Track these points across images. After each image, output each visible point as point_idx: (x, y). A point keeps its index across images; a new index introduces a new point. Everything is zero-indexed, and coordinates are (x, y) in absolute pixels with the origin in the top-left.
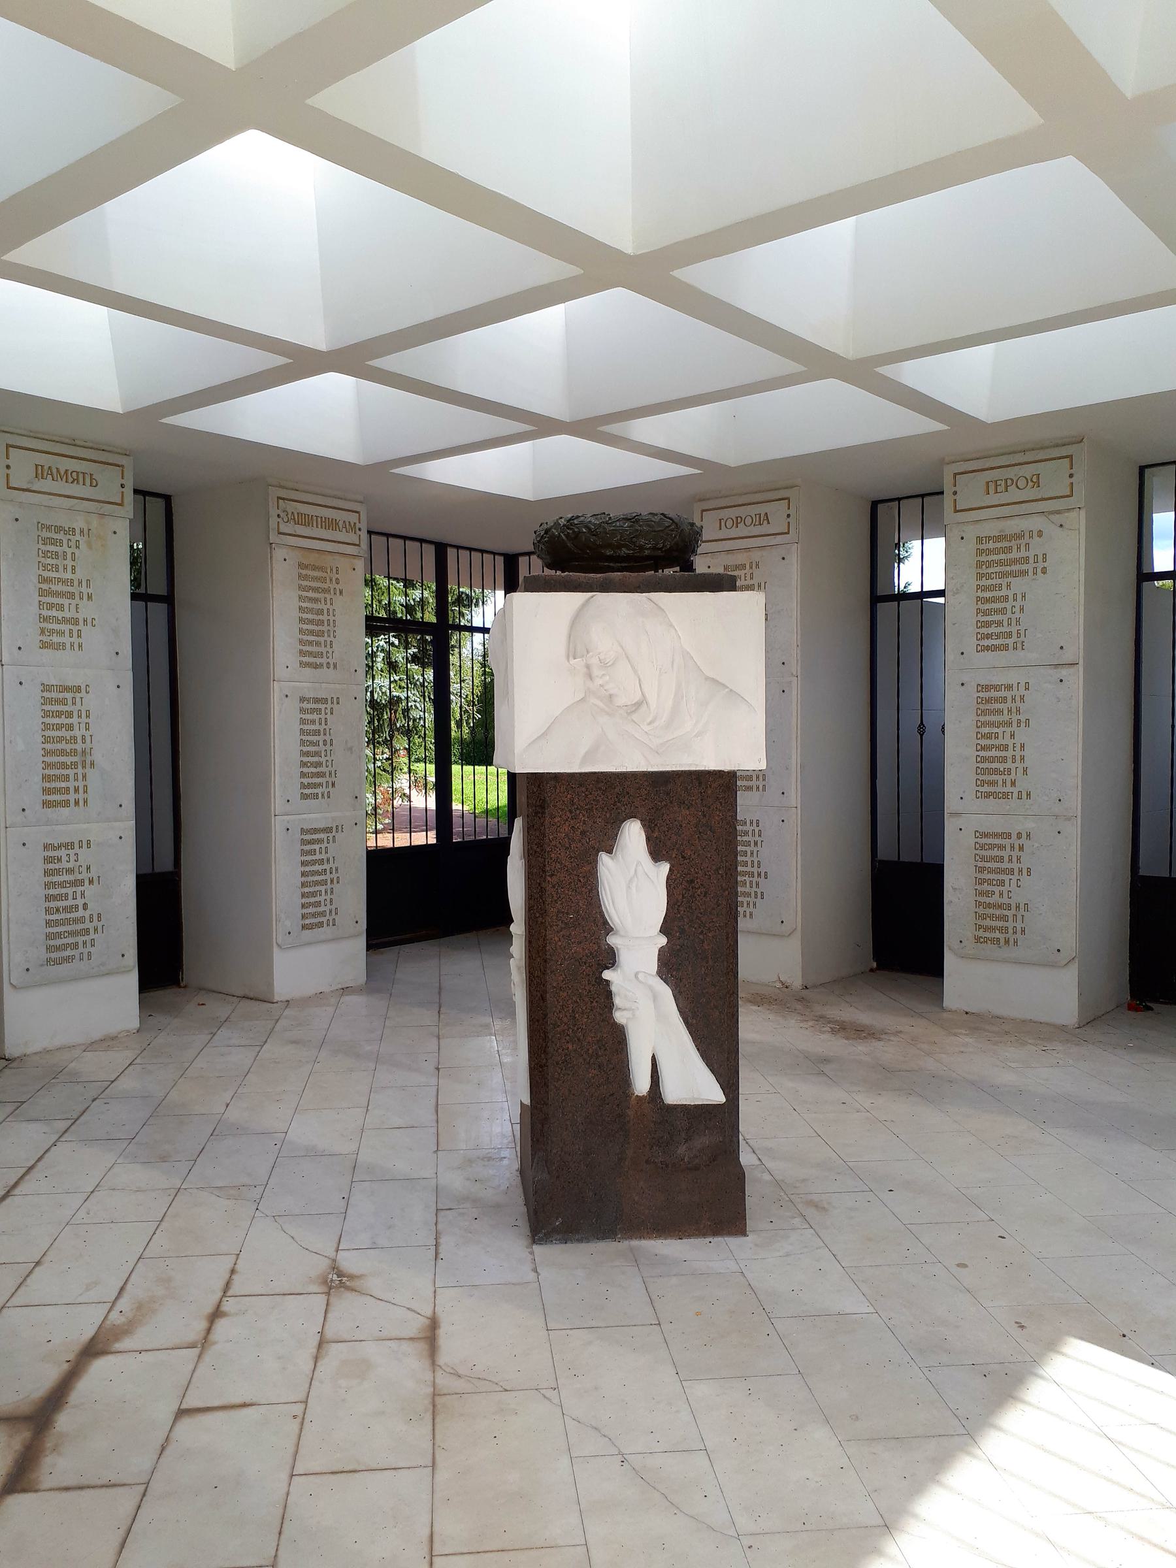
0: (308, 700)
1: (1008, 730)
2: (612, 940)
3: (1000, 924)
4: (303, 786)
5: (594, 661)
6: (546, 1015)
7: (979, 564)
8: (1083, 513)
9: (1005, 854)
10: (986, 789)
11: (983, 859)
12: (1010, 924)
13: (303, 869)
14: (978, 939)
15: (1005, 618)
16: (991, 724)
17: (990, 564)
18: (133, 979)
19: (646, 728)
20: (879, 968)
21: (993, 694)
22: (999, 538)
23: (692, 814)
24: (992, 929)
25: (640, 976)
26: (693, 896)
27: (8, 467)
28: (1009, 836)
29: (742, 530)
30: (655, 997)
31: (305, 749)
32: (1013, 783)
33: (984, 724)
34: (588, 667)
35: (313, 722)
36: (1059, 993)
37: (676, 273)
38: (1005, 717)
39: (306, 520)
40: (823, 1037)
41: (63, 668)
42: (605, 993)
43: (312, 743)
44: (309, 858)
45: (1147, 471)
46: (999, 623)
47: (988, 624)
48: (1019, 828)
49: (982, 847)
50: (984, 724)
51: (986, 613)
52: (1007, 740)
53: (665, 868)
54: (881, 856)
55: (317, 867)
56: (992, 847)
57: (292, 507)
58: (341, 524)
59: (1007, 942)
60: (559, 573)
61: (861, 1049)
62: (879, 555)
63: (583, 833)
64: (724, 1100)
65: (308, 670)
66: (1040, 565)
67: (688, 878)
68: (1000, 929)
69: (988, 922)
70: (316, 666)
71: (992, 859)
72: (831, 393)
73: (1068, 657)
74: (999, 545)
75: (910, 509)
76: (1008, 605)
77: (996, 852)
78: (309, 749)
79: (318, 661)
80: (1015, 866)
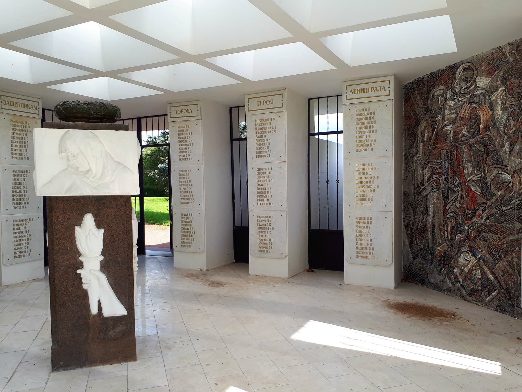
0: (16, 172)
1: (266, 183)
2: (81, 258)
3: (265, 246)
4: (14, 204)
5: (69, 154)
6: (55, 288)
7: (256, 129)
8: (286, 112)
9: (266, 223)
10: (260, 202)
11: (260, 225)
12: (268, 246)
13: (14, 235)
14: (259, 251)
15: (264, 147)
16: (261, 181)
17: (259, 129)
19: (92, 180)
20: (236, 262)
21: (261, 171)
22: (262, 120)
23: (110, 211)
24: (263, 247)
25: (92, 271)
26: (113, 241)
28: (267, 217)
29: (183, 114)
30: (98, 279)
31: (14, 190)
32: (268, 200)
33: (259, 181)
34: (68, 156)
35: (18, 180)
36: (281, 267)
37: (111, 17)
38: (265, 179)
39: (15, 104)
40: (205, 287)
42: (79, 278)
43: (18, 188)
44: (17, 231)
45: (311, 100)
46: (263, 148)
47: (259, 149)
48: (270, 215)
49: (260, 221)
50: (259, 181)
51: (259, 145)
52: (266, 186)
53: (102, 231)
54: (236, 225)
55: (21, 234)
56: (262, 221)
57: (7, 99)
58: (30, 106)
59: (267, 251)
60: (64, 122)
61: (215, 290)
63: (69, 219)
65: (16, 160)
66: (274, 129)
67: (112, 234)
68: (265, 247)
69: (262, 245)
70: (19, 159)
71: (263, 225)
72: (191, 68)
73: (283, 159)
74: (262, 123)
76: (265, 142)
77: (263, 223)
78: (16, 190)
79: (20, 157)
80: (269, 227)
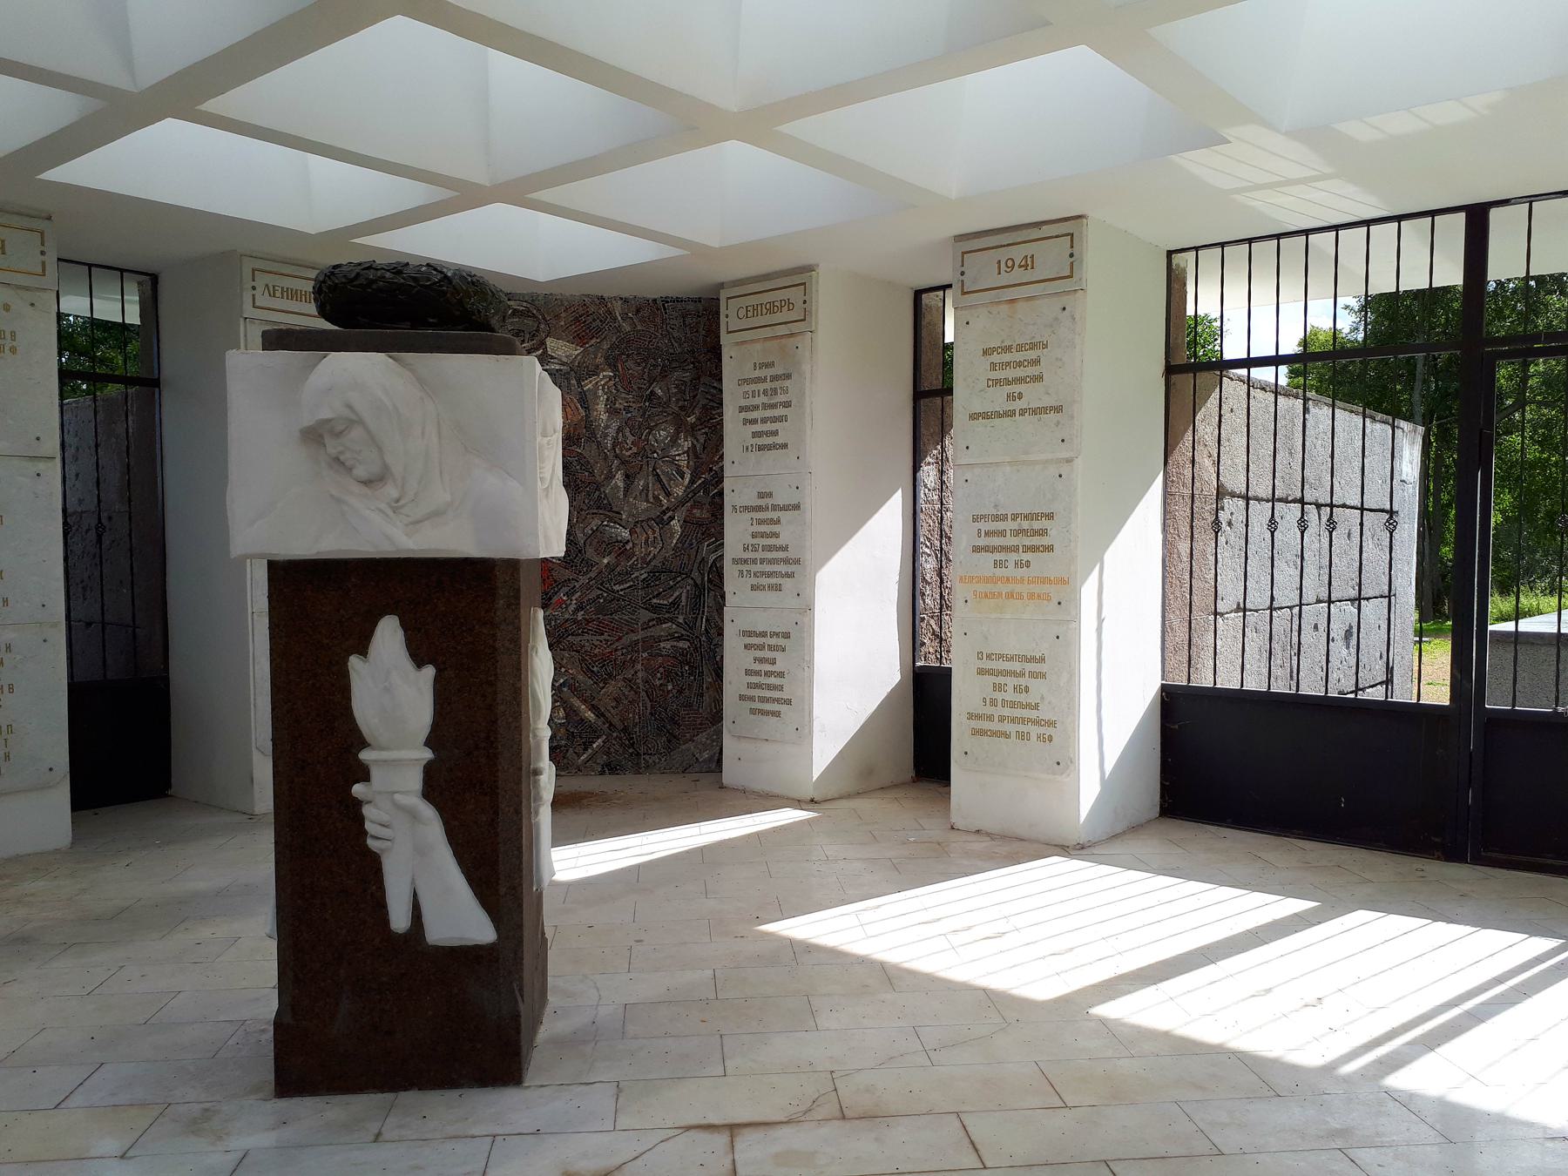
2: (365, 755)
18: (63, 795)
23: (454, 607)
27: (43, 253)
53: (429, 672)
75: (1210, 258)
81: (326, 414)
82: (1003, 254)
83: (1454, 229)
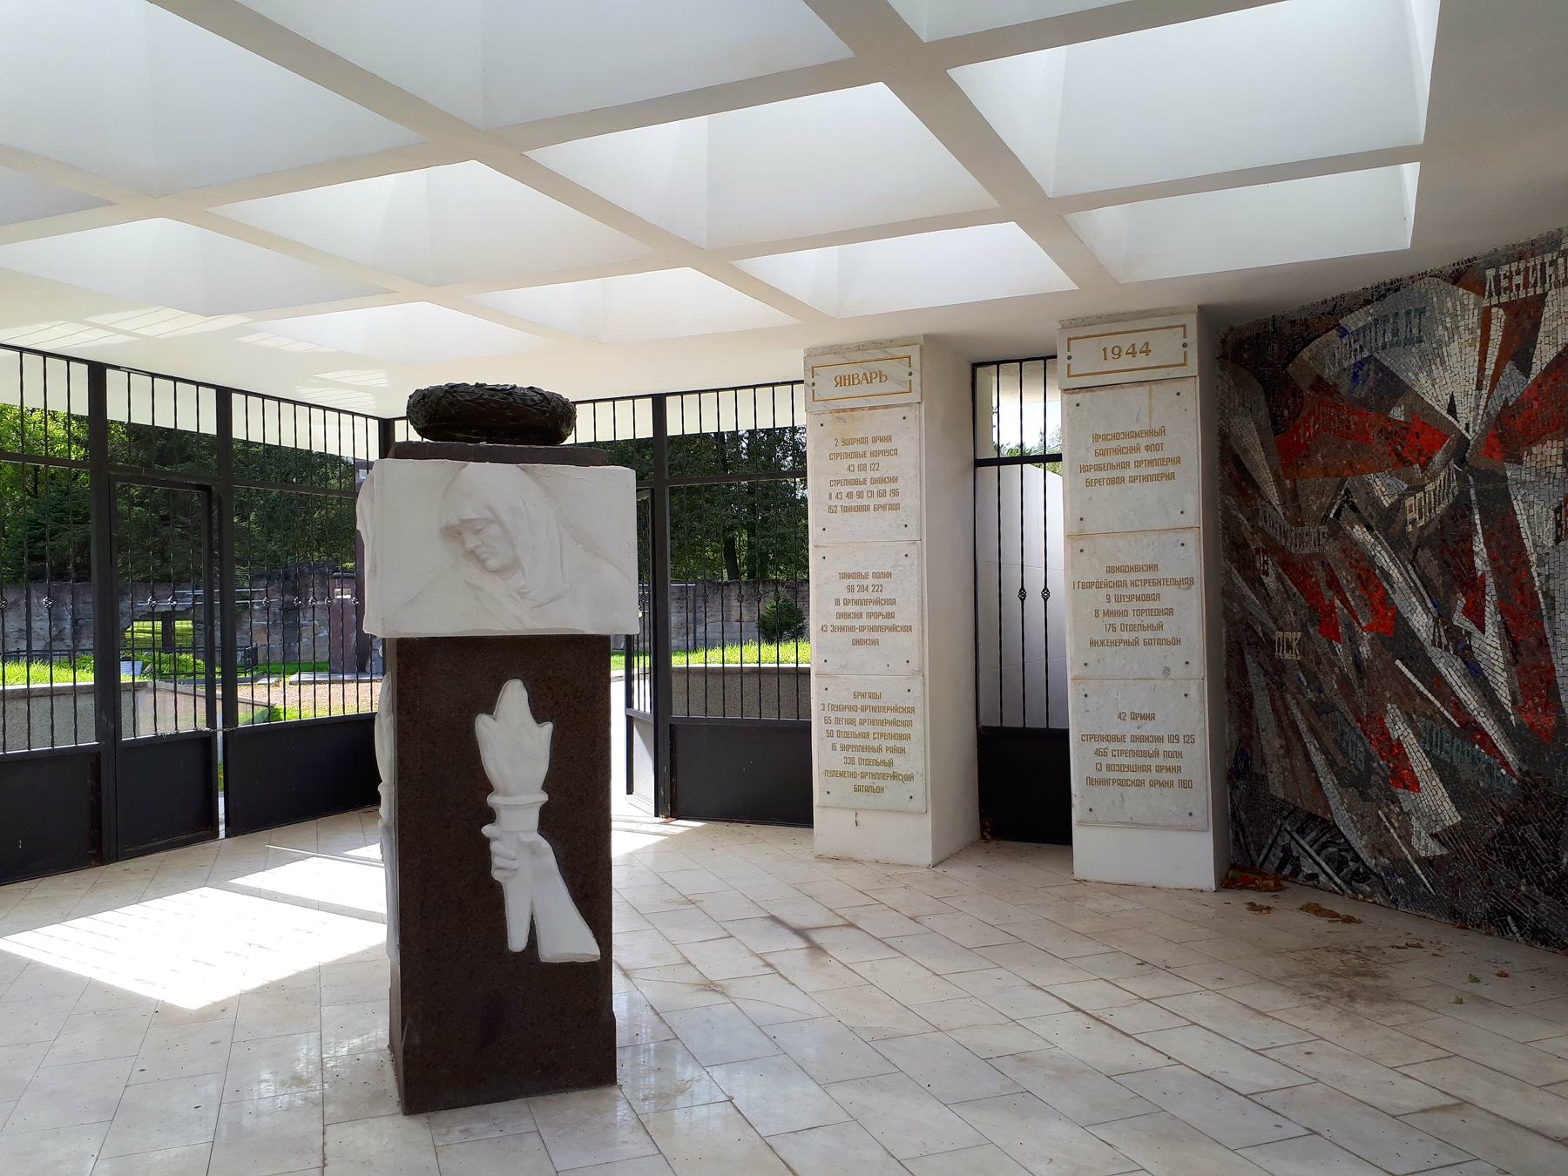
2: (492, 800)
23: (566, 674)
41: (1128, 739)
62: (976, 414)
64: (598, 952)
81: (470, 514)
82: (1109, 342)
83: (646, 407)
